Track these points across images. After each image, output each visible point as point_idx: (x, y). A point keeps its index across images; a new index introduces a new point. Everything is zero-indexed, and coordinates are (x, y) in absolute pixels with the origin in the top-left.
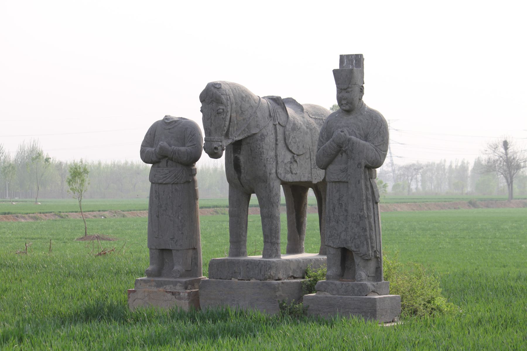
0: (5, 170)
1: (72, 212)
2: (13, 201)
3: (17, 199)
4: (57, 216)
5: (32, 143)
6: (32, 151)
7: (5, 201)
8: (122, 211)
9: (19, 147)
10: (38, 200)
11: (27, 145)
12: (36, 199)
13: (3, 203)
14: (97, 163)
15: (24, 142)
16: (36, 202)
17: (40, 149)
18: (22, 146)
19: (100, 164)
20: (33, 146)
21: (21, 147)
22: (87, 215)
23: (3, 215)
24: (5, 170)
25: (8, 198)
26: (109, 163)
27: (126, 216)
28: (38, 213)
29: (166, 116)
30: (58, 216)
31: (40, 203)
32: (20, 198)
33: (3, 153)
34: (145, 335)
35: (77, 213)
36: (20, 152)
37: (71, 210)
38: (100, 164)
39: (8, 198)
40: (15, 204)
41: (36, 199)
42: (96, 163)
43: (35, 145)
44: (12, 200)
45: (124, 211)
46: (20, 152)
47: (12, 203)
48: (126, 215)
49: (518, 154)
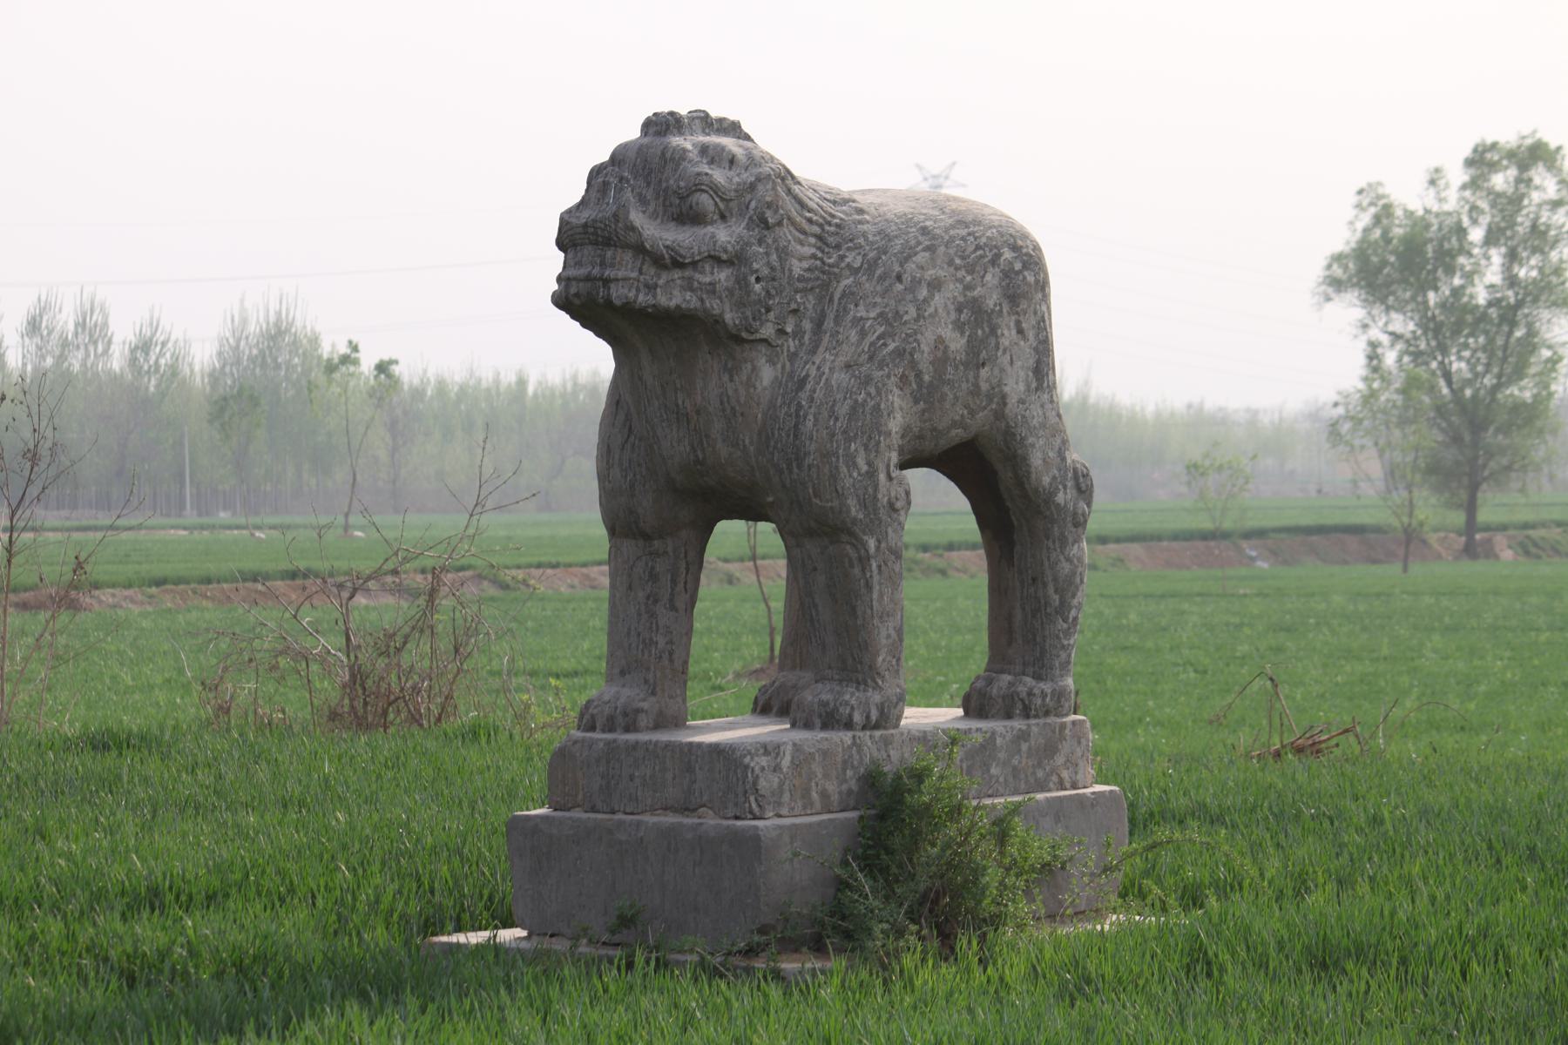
0: (222, 410)
1: (539, 566)
2: (259, 528)
3: (224, 516)
4: (486, 583)
5: (274, 306)
6: (273, 338)
7: (212, 527)
8: (719, 559)
9: (225, 319)
10: (352, 520)
11: (255, 315)
12: (347, 515)
13: (205, 533)
14: (513, 378)
15: (242, 301)
16: (346, 528)
17: (309, 329)
18: (236, 319)
19: (522, 383)
20: (279, 314)
21: (233, 321)
22: (593, 575)
23: (288, 582)
24: (222, 410)
25: (190, 517)
26: (555, 378)
27: (738, 579)
28: (415, 571)
29: (660, 125)
30: (490, 581)
31: (359, 534)
32: (234, 514)
33: (164, 344)
34: (860, 958)
35: (557, 571)
36: (231, 341)
37: (535, 560)
38: (522, 383)
39: (190, 517)
40: (262, 536)
41: (347, 515)
42: (509, 378)
43: (287, 310)
44: (253, 520)
45: (726, 560)
46: (231, 341)
47: (253, 535)
48: (738, 574)
49: (1398, 456)
